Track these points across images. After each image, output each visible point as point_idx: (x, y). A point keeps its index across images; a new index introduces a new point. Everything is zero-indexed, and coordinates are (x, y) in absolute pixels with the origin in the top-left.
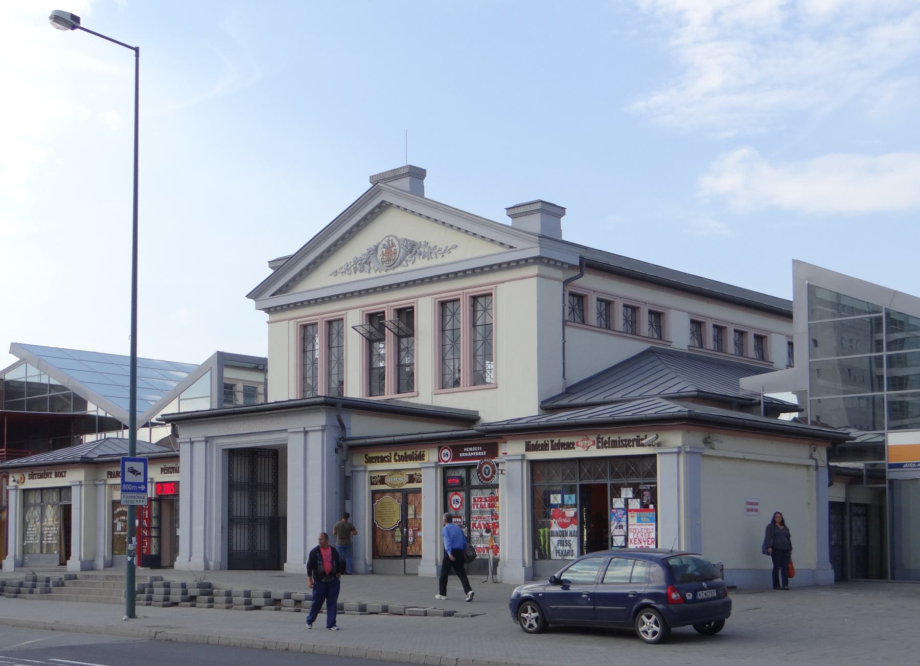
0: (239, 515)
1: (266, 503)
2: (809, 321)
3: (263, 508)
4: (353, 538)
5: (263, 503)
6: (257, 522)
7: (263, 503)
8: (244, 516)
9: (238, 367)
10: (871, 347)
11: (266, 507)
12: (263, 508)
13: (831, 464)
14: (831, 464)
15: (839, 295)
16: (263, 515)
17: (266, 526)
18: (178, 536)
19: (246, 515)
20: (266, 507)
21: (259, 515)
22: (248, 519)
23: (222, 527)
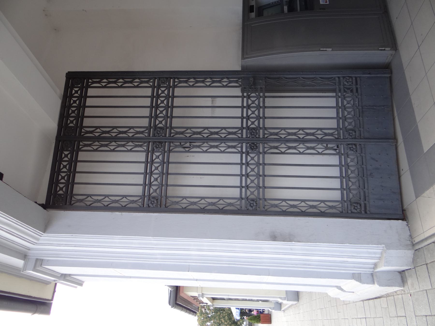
0: (236, 181)
1: (208, 102)
2: (243, 58)
3: (219, 112)
4: (401, 279)
5: (208, 112)
6: (258, 128)
7: (208, 112)
8: (241, 164)
9: (42, 282)
10: (249, 12)
11: (219, 102)
12: (219, 112)
13: (335, 81)
14: (335, 81)
15: (349, 301)
16: (238, 112)
17: (269, 102)
18: (68, 72)
19: (236, 158)
20: (219, 102)
21: (237, 123)
22: (247, 153)
23: (274, 238)
